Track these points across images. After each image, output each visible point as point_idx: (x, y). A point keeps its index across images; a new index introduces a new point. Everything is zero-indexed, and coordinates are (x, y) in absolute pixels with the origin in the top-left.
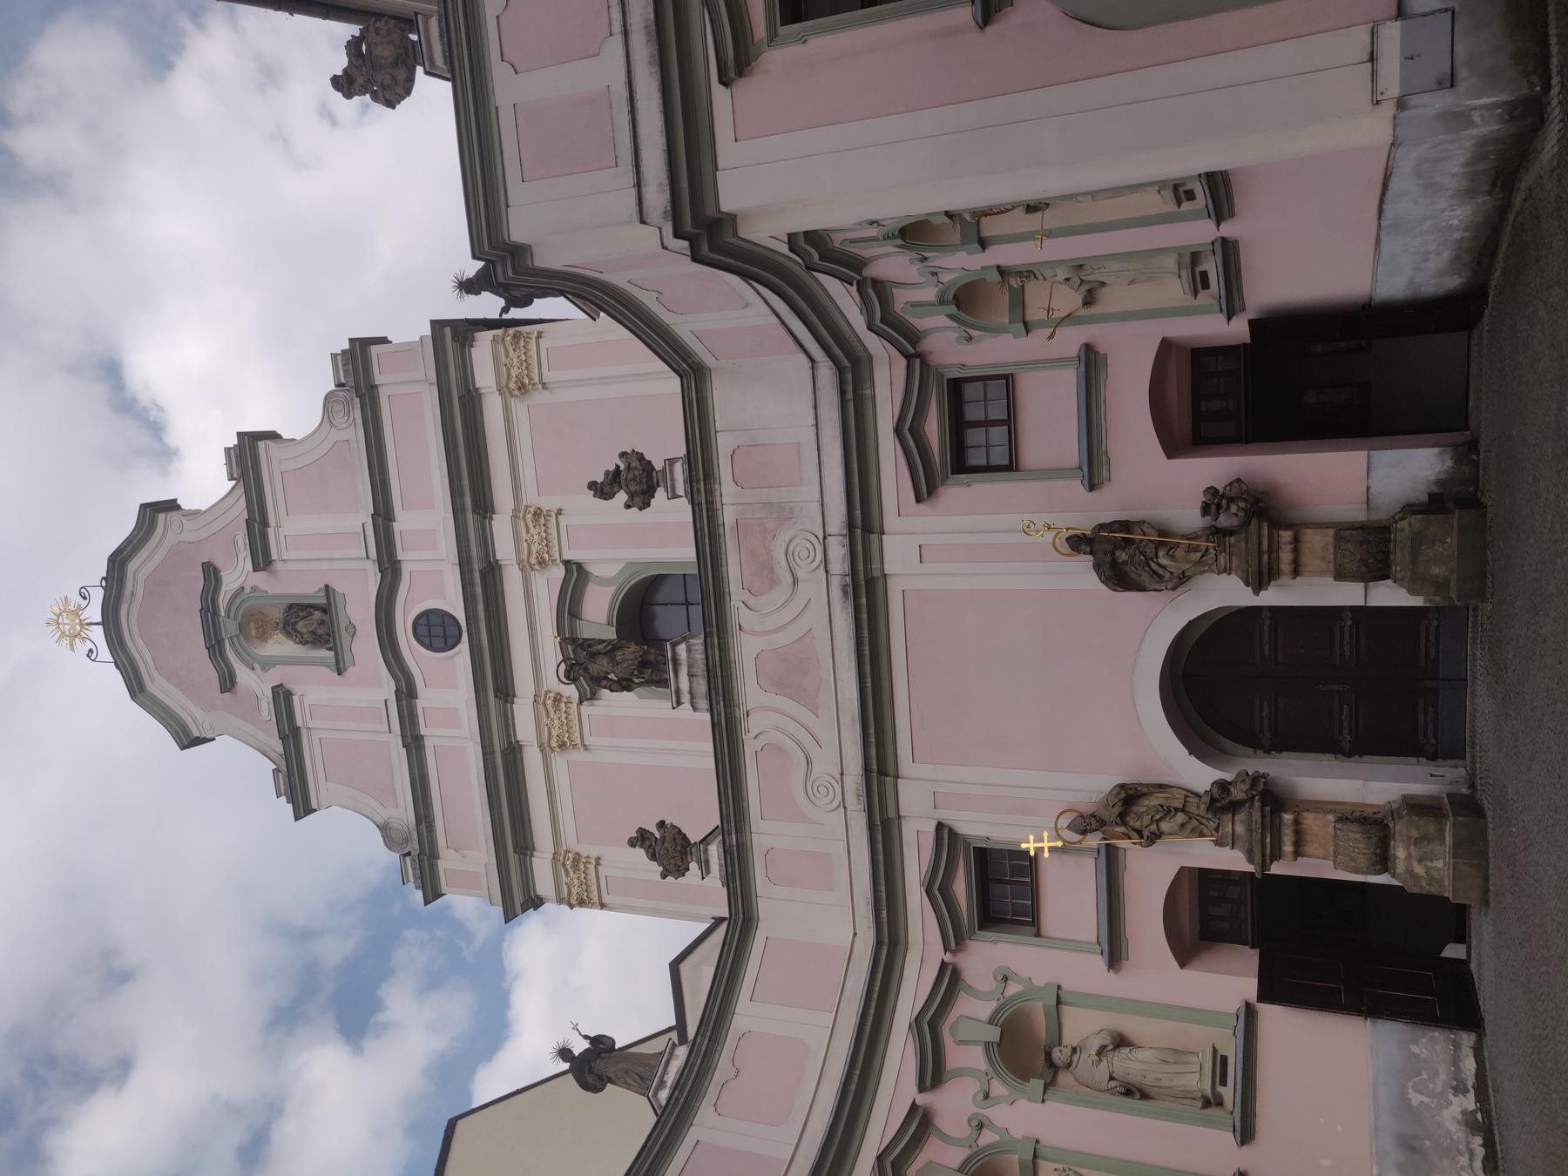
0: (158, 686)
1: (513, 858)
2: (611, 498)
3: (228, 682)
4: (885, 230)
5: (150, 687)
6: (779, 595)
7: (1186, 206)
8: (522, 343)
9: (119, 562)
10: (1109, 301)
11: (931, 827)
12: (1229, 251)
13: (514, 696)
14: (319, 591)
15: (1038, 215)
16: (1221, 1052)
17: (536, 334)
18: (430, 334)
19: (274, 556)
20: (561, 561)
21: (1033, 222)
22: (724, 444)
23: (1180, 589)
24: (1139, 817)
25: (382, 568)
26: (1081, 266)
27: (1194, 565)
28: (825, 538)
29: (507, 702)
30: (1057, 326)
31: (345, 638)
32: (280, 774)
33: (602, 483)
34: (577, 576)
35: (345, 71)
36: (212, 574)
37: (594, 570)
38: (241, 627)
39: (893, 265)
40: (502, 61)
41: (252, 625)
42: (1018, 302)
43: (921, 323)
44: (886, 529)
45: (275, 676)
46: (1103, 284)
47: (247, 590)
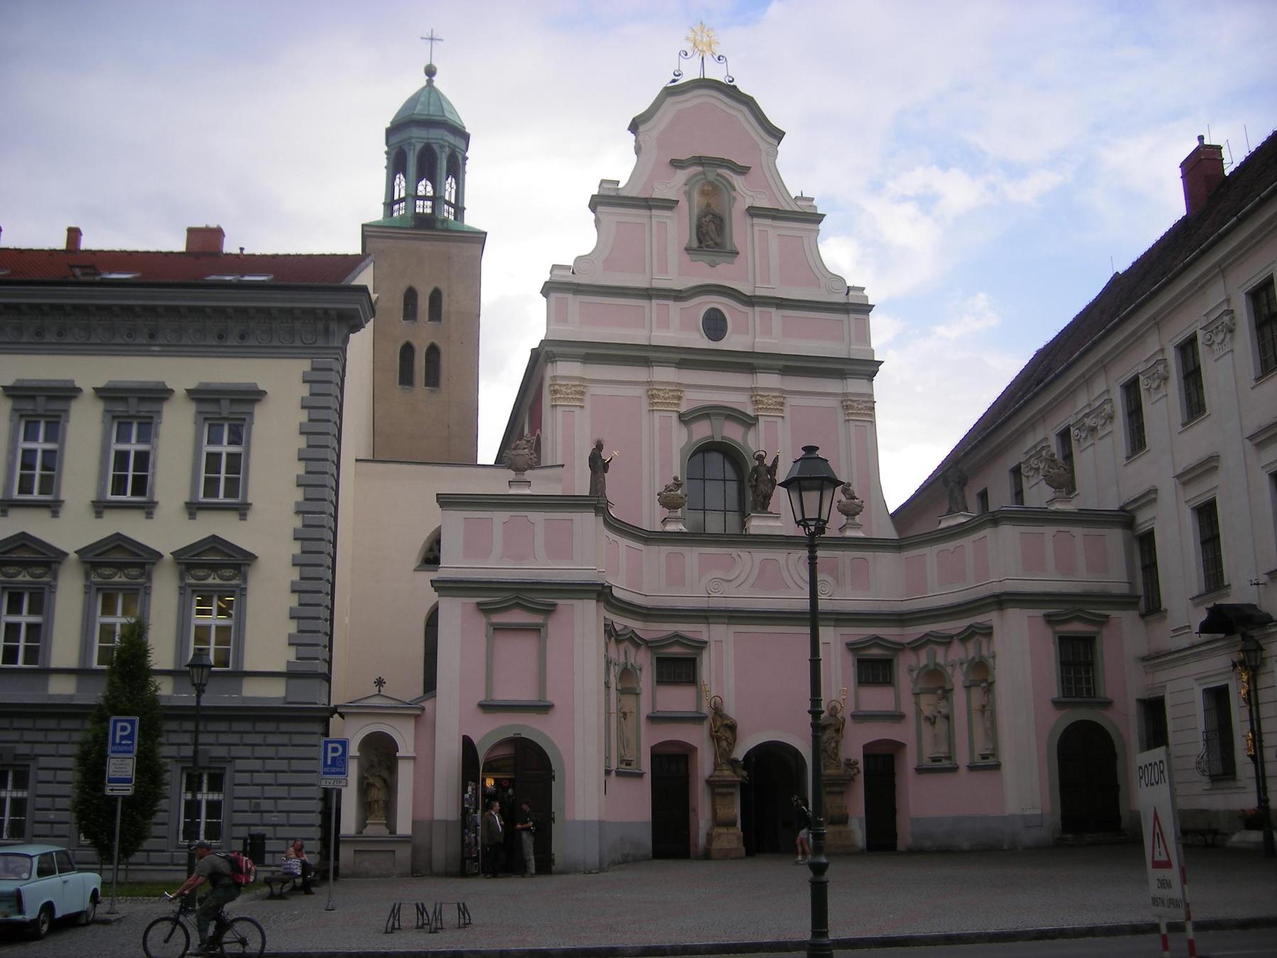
0: (673, 106)
1: (583, 351)
3: (676, 164)
5: (670, 100)
10: (926, 730)
11: (705, 638)
12: (954, 769)
14: (735, 246)
16: (633, 763)
18: (875, 359)
19: (756, 220)
20: (758, 415)
22: (868, 555)
26: (947, 718)
33: (849, 489)
34: (749, 422)
36: (743, 170)
37: (751, 434)
38: (711, 183)
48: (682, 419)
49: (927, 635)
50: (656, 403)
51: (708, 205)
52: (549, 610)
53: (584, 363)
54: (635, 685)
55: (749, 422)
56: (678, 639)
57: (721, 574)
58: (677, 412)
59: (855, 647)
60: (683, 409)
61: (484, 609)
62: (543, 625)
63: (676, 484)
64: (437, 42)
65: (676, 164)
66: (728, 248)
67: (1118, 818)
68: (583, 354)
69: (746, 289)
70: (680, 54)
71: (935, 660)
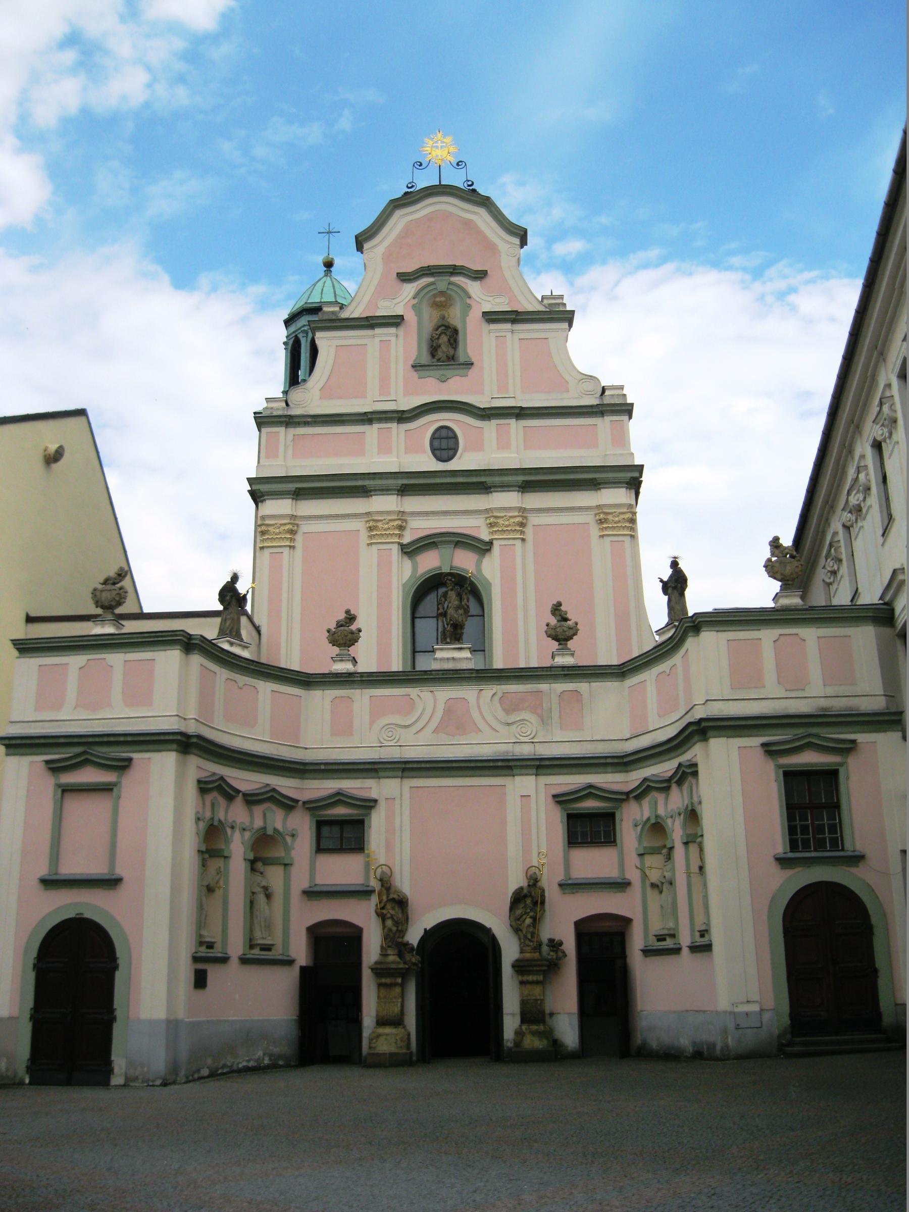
0: (400, 220)
1: (292, 486)
2: (552, 614)
3: (404, 278)
4: (696, 804)
5: (398, 213)
6: (500, 713)
7: (697, 934)
8: (627, 524)
9: (486, 202)
10: (652, 895)
11: (374, 795)
12: (677, 951)
13: (402, 496)
14: (470, 359)
15: (697, 870)
16: (273, 948)
17: (633, 534)
18: (636, 464)
20: (493, 539)
21: (695, 868)
22: (583, 687)
23: (509, 927)
24: (393, 909)
25: (486, 410)
26: (671, 884)
27: (524, 935)
28: (533, 742)
29: (398, 491)
30: (642, 870)
31: (439, 373)
32: (337, 309)
34: (483, 548)
35: (781, 545)
36: (480, 275)
38: (442, 293)
39: (677, 799)
40: (780, 635)
41: (443, 299)
42: (654, 851)
43: (646, 803)
44: (538, 777)
45: (411, 318)
46: (661, 892)
47: (468, 301)
48: (405, 550)
49: (645, 780)
50: (374, 535)
51: (443, 318)
52: (124, 765)
53: (296, 500)
54: (223, 847)
55: (483, 548)
56: (339, 798)
57: (397, 719)
58: (399, 543)
59: (561, 799)
60: (407, 540)
61: (54, 768)
62: (115, 784)
63: (348, 618)
64: (325, 231)
65: (404, 278)
66: (462, 359)
67: (879, 1014)
68: (294, 489)
69: (482, 401)
70: (414, 165)
71: (656, 812)
